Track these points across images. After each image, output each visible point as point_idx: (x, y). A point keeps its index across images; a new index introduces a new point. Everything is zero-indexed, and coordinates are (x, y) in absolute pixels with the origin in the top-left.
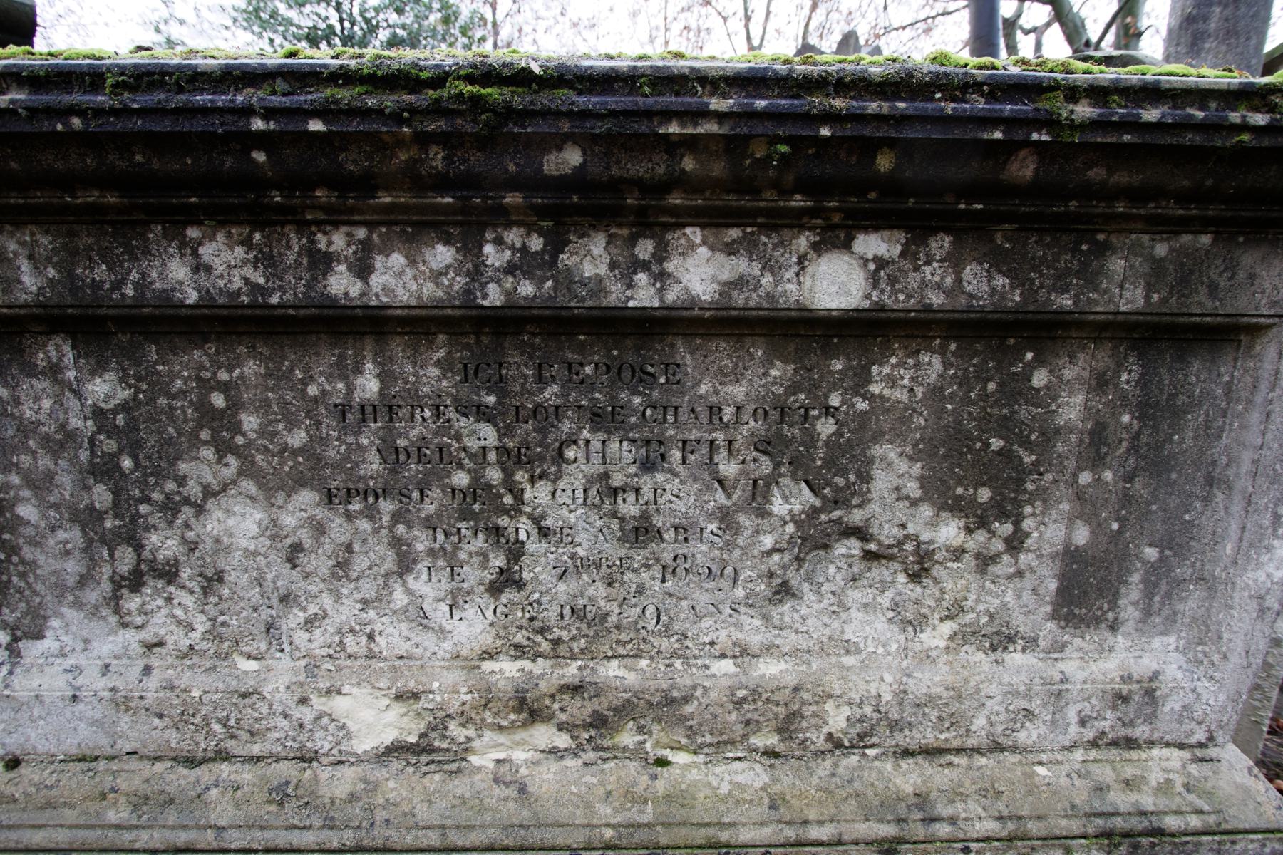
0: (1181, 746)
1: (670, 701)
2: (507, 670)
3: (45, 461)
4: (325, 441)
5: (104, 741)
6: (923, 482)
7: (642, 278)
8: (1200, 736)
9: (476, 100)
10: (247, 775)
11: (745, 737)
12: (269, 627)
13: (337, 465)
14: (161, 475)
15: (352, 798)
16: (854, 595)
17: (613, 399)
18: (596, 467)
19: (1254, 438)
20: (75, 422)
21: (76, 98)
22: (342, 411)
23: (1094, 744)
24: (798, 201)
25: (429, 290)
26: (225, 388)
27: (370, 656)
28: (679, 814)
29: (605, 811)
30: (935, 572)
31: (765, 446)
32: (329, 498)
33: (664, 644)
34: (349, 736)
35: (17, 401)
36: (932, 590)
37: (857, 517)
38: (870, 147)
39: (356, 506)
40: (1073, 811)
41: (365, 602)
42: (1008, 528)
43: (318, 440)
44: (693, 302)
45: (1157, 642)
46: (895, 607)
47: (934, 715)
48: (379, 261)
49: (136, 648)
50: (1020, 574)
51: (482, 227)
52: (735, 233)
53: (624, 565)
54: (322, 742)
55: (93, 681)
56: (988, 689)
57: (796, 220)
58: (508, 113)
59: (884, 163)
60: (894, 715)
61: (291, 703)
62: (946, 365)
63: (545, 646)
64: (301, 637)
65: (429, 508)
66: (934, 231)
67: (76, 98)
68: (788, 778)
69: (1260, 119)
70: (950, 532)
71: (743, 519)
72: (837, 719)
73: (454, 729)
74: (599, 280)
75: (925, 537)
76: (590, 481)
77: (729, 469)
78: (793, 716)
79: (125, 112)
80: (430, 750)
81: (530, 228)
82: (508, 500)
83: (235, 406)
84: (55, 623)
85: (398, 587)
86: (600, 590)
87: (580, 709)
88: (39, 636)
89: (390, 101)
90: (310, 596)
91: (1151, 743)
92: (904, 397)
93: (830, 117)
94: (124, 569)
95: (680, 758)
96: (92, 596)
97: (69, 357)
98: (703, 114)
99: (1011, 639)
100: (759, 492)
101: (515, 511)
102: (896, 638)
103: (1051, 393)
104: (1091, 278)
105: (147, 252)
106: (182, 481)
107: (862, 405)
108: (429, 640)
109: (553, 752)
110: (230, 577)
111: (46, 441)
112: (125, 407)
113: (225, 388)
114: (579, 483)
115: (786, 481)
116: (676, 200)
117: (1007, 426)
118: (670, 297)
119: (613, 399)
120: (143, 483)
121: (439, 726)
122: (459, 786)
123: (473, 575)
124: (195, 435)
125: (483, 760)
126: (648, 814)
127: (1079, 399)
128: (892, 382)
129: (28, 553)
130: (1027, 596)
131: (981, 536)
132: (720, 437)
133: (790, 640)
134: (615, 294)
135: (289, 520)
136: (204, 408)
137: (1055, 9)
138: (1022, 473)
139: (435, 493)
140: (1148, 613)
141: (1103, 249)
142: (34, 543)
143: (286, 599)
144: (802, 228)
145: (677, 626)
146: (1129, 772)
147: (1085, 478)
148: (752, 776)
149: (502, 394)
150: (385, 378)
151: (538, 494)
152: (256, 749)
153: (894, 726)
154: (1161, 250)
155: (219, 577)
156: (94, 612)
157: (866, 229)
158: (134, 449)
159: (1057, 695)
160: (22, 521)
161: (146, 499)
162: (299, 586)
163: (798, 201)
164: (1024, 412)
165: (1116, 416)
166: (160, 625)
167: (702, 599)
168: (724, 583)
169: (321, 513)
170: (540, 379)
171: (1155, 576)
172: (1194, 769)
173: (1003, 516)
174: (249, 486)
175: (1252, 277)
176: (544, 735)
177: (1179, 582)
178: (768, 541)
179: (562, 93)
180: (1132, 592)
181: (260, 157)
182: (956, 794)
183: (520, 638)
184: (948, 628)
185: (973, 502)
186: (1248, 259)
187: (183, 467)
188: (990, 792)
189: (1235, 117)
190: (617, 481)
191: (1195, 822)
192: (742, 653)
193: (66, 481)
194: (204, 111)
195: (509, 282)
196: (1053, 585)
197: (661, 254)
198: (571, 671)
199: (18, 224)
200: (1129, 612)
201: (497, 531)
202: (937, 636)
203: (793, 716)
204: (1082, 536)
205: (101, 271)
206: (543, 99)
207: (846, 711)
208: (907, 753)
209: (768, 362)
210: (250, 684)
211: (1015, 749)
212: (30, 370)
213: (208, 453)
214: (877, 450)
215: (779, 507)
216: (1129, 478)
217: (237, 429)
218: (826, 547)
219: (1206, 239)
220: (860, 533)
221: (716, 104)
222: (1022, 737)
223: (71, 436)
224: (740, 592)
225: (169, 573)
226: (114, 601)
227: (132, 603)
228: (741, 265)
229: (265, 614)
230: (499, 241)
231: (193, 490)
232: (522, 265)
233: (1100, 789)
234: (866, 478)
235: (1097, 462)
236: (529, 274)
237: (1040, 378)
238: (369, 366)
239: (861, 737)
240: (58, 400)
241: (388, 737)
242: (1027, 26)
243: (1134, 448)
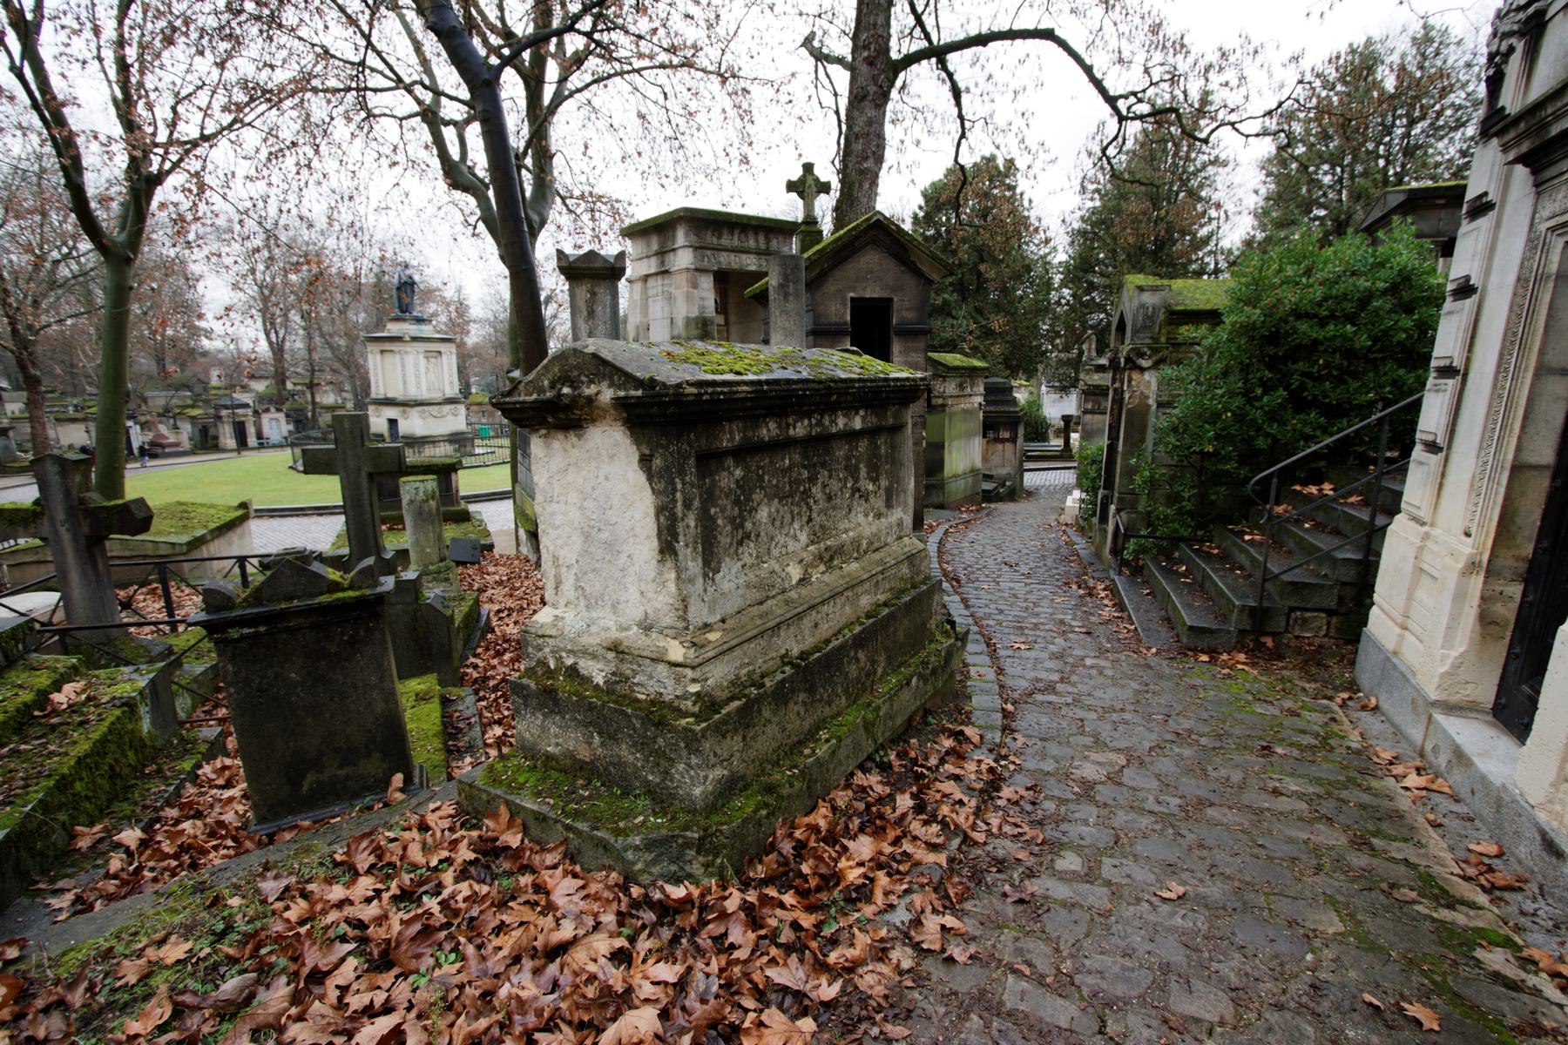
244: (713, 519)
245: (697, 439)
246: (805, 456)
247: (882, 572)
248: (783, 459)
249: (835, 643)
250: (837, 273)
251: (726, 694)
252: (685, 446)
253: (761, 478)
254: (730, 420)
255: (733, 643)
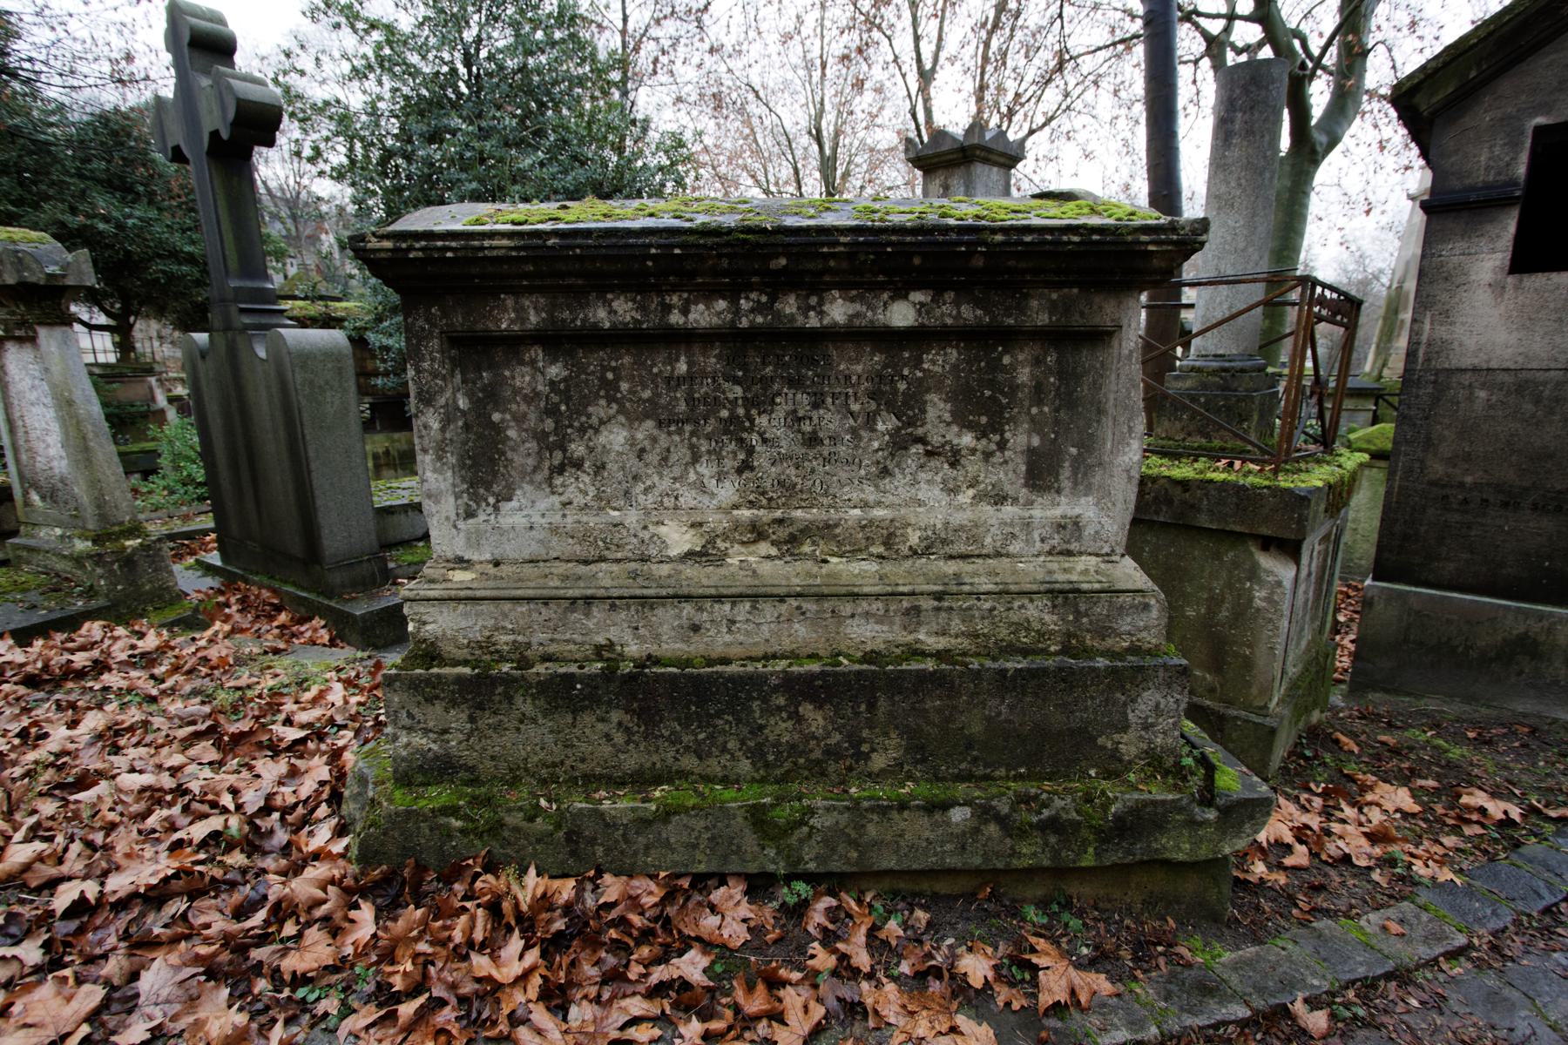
0: (1097, 555)
1: (828, 526)
2: (746, 514)
3: (523, 407)
4: (659, 395)
5: (543, 552)
6: (953, 413)
7: (812, 313)
8: (1106, 549)
9: (745, 241)
10: (615, 568)
11: (867, 547)
12: (627, 493)
13: (665, 407)
14: (579, 413)
15: (669, 576)
16: (922, 476)
17: (798, 373)
18: (790, 407)
19: (1113, 387)
20: (540, 388)
21: (579, 241)
22: (668, 380)
23: (1050, 553)
24: (881, 278)
25: (715, 320)
26: (614, 370)
27: (676, 508)
28: (833, 582)
29: (796, 581)
30: (963, 461)
31: (872, 395)
32: (660, 424)
33: (825, 501)
34: (667, 547)
35: (513, 378)
36: (962, 472)
37: (920, 431)
38: (911, 255)
39: (673, 428)
40: (1035, 582)
41: (675, 479)
42: (997, 438)
43: (657, 395)
44: (836, 324)
45: (1083, 500)
46: (944, 482)
47: (964, 536)
48: (693, 307)
49: (558, 506)
50: (1006, 462)
51: (740, 292)
52: (854, 292)
53: (805, 458)
54: (653, 551)
55: (537, 519)
56: (990, 522)
57: (882, 287)
58: (758, 245)
59: (917, 261)
60: (943, 535)
61: (639, 528)
62: (960, 354)
63: (764, 502)
64: (641, 498)
65: (709, 429)
66: (946, 290)
67: (579, 241)
68: (888, 567)
69: (1076, 239)
70: (967, 439)
71: (863, 433)
72: (914, 538)
73: (721, 544)
74: (792, 315)
75: (955, 442)
76: (788, 414)
77: (855, 407)
78: (891, 535)
79: (601, 246)
80: (707, 554)
81: (761, 292)
82: (747, 424)
83: (618, 379)
84: (518, 492)
85: (692, 471)
86: (792, 471)
87: (783, 533)
88: (510, 499)
89: (710, 241)
90: (648, 476)
91: (1081, 553)
92: (939, 370)
93: (890, 244)
94: (556, 463)
95: (834, 560)
96: (539, 477)
97: (541, 356)
98: (838, 243)
99: (1005, 498)
100: (870, 420)
101: (751, 430)
102: (945, 499)
103: (1013, 367)
104: (1022, 309)
105: (588, 305)
106: (589, 416)
107: (919, 374)
108: (706, 499)
109: (768, 557)
110: (609, 466)
111: (525, 398)
112: (565, 380)
113: (614, 370)
114: (782, 415)
115: (884, 413)
116: (827, 278)
117: (992, 384)
118: (825, 322)
119: (798, 373)
120: (570, 418)
121: (711, 542)
122: (722, 571)
123: (729, 464)
124: (597, 393)
125: (733, 561)
126: (818, 581)
127: (1027, 370)
128: (934, 362)
129: (509, 454)
130: (1011, 474)
131: (984, 442)
132: (850, 391)
133: (889, 499)
134: (800, 320)
135: (640, 436)
136: (603, 379)
137: (1265, 30)
138: (1002, 408)
139: (712, 421)
140: (1076, 484)
141: (1026, 297)
142: (513, 450)
143: (636, 478)
144: (885, 290)
145: (831, 491)
146: (1067, 565)
147: (1034, 410)
148: (872, 567)
149: (746, 371)
150: (690, 364)
151: (762, 421)
152: (619, 555)
153: (944, 542)
154: (1054, 296)
155: (603, 466)
156: (539, 487)
157: (914, 289)
158: (567, 401)
159: (1027, 525)
160: (508, 438)
161: (571, 426)
162: (642, 471)
163: (881, 278)
164: (1000, 377)
165: (1047, 378)
166: (571, 493)
167: (843, 475)
168: (855, 468)
169: (656, 432)
170: (764, 363)
171: (1077, 463)
172: (1103, 566)
173: (994, 431)
174: (622, 419)
175: (1101, 308)
176: (764, 548)
177: (1091, 467)
178: (876, 445)
179: (780, 236)
180: (1066, 472)
181: (650, 263)
182: (975, 574)
183: (751, 497)
184: (971, 492)
185: (978, 423)
186: (1097, 299)
187: (590, 409)
188: (992, 573)
189: (1065, 238)
190: (801, 413)
191: (1097, 586)
192: (865, 505)
193: (532, 417)
194: (632, 246)
195: (751, 317)
196: (1024, 468)
197: (821, 303)
198: (778, 514)
199: (531, 294)
200: (1066, 484)
201: (741, 441)
202: (966, 496)
203: (891, 535)
204: (1036, 441)
205: (566, 314)
206: (772, 240)
207: (918, 533)
208: (951, 557)
209: (873, 354)
210: (618, 521)
211: (1008, 555)
212: (522, 363)
213: (603, 402)
214: (928, 397)
215: (880, 427)
216: (1057, 410)
217: (618, 389)
218: (906, 448)
219: (1075, 291)
220: (922, 440)
221: (843, 239)
222: (1011, 549)
223: (537, 394)
224: (863, 472)
225: (578, 464)
226: (549, 480)
227: (558, 481)
228: (858, 307)
229: (625, 485)
230: (747, 298)
231: (594, 421)
232: (758, 308)
233: (1050, 572)
234: (924, 411)
235: (1039, 402)
236: (761, 313)
237: (1006, 360)
238: (683, 358)
239: (927, 548)
240: (533, 377)
241: (686, 548)
242: (1240, 44)
243: (1058, 395)
244: (498, 429)
245: (445, 315)
246: (731, 361)
247: (939, 596)
248: (672, 361)
249: (734, 668)
250: (1505, 86)
251: (463, 654)
252: (421, 323)
253: (613, 386)
254: (517, 292)
255: (479, 594)
